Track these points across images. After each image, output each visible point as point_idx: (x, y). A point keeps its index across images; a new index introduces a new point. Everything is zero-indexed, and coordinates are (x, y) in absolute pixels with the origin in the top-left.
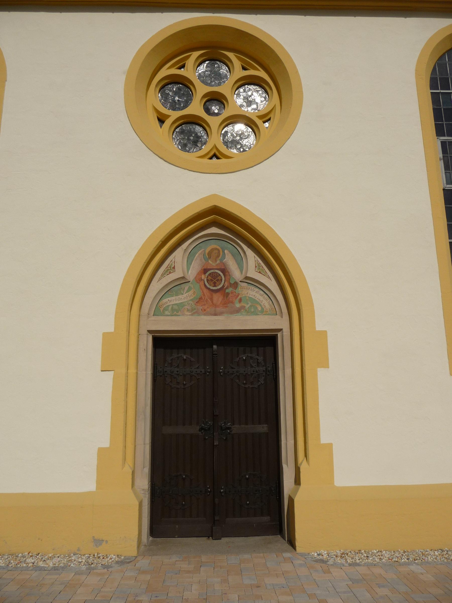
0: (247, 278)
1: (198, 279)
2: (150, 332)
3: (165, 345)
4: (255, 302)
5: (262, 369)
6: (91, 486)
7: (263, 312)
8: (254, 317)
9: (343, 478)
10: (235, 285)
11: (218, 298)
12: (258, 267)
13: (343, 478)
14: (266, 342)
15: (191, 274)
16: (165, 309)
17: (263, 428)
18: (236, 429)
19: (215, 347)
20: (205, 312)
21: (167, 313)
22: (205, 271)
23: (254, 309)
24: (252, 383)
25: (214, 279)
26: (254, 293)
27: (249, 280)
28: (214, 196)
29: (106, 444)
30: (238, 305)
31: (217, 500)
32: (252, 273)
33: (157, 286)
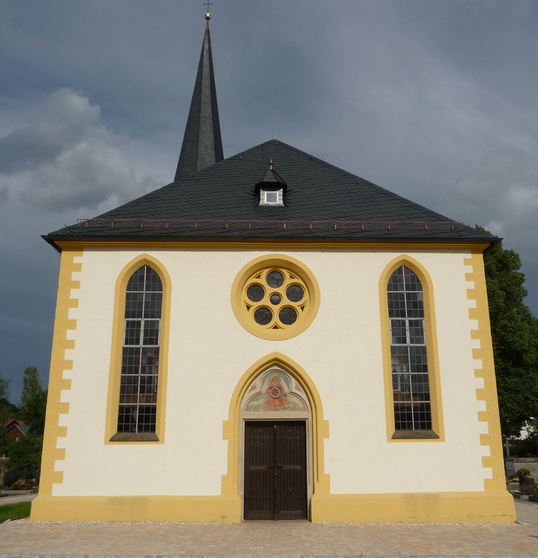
0: (291, 392)
1: (267, 392)
2: (244, 419)
3: (251, 426)
4: (295, 404)
5: (298, 437)
6: (219, 493)
7: (299, 409)
8: (295, 412)
9: (335, 490)
10: (286, 395)
11: (277, 402)
12: (297, 386)
13: (335, 490)
14: (301, 424)
15: (264, 389)
16: (251, 408)
17: (299, 467)
18: (286, 467)
19: (275, 426)
20: (271, 410)
21: (252, 409)
22: (271, 388)
23: (294, 408)
24: (293, 445)
25: (275, 392)
26: (295, 400)
27: (292, 393)
28: (276, 353)
29: (225, 473)
30: (287, 406)
31: (276, 502)
32: (294, 390)
33: (247, 396)
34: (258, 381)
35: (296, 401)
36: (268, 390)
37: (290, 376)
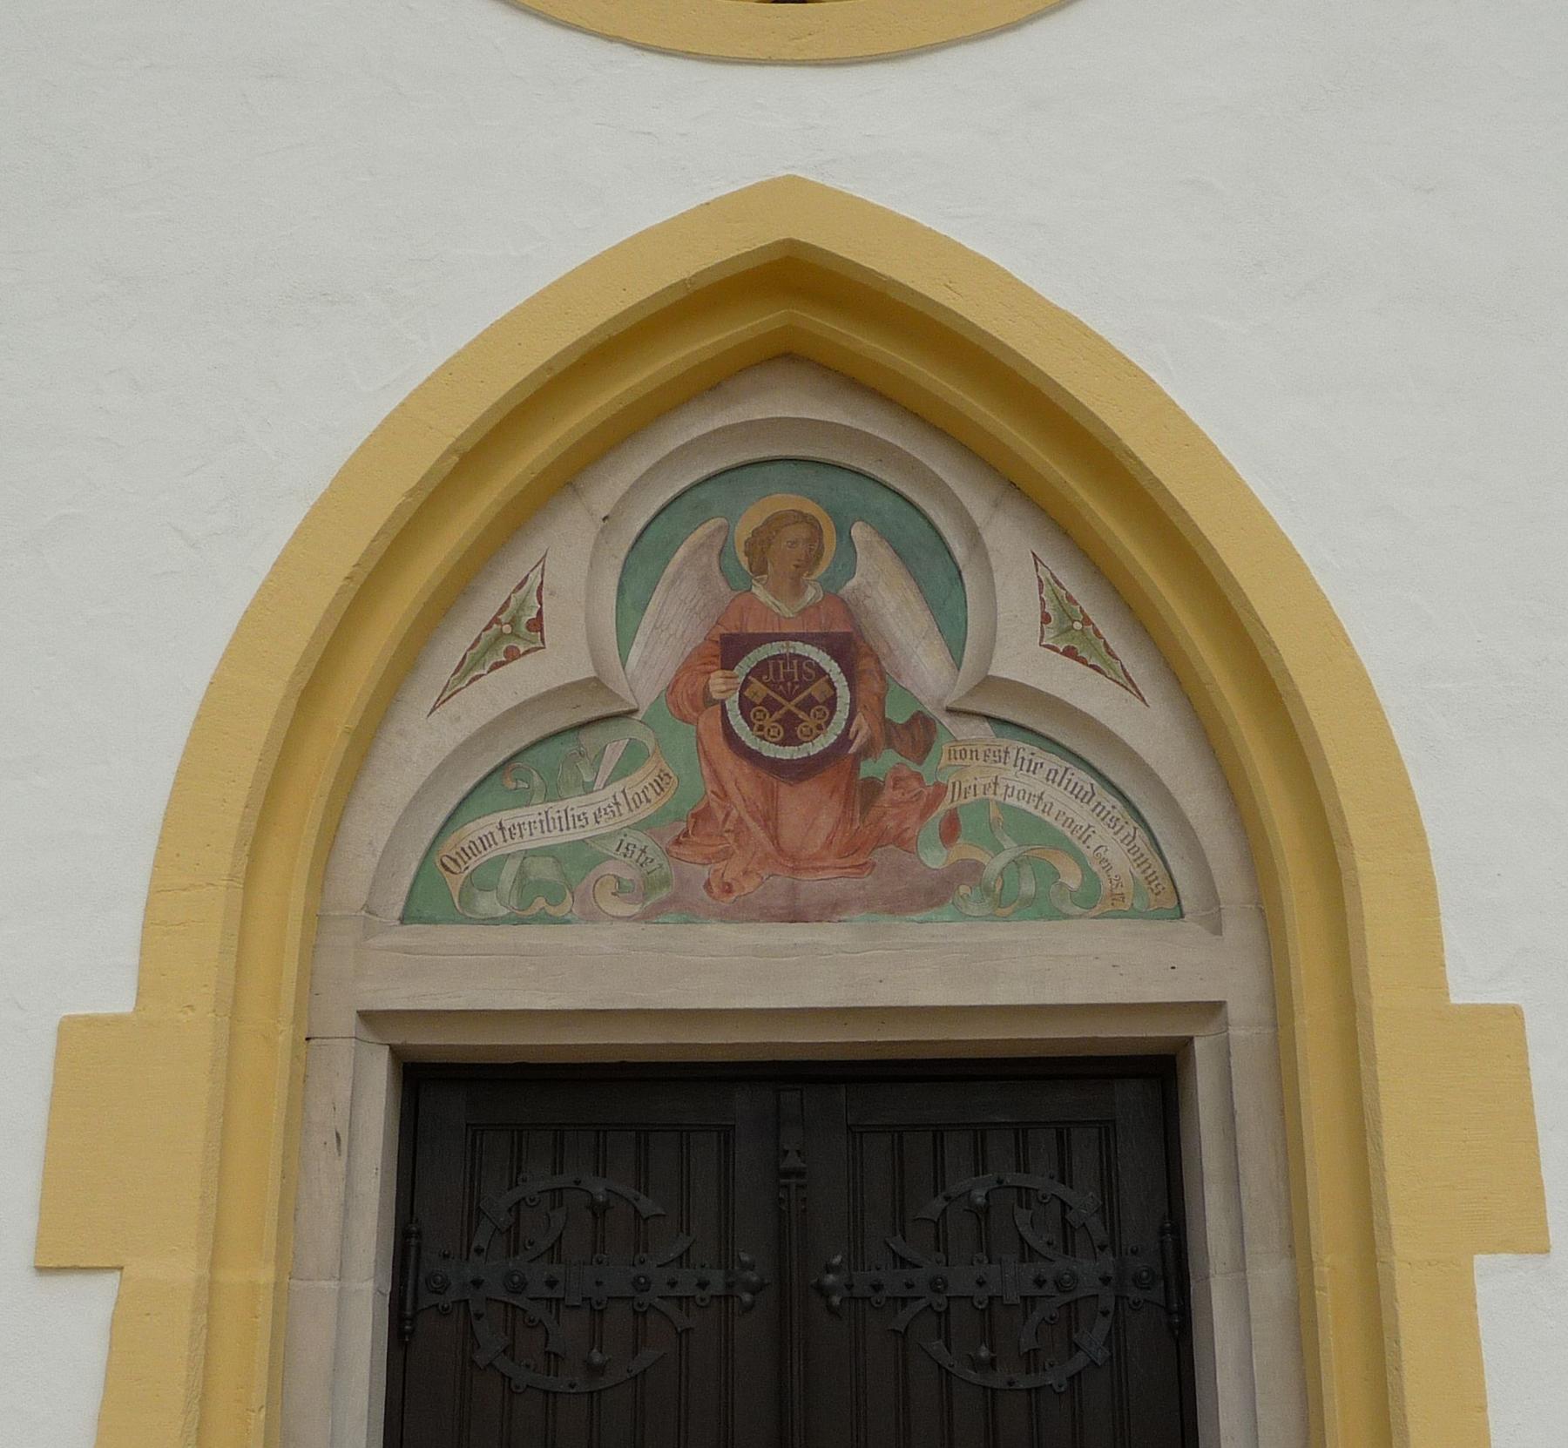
0: (988, 684)
1: (687, 698)
4: (1032, 829)
5: (1088, 1269)
7: (1095, 900)
10: (919, 733)
11: (809, 815)
14: (1104, 1118)
15: (650, 665)
20: (727, 902)
21: (486, 904)
22: (730, 648)
23: (1038, 887)
24: (1031, 1361)
25: (786, 695)
26: (1027, 784)
28: (789, 189)
30: (935, 858)
32: (1021, 655)
33: (432, 737)
34: (571, 564)
35: (1058, 797)
36: (695, 665)
37: (977, 504)
